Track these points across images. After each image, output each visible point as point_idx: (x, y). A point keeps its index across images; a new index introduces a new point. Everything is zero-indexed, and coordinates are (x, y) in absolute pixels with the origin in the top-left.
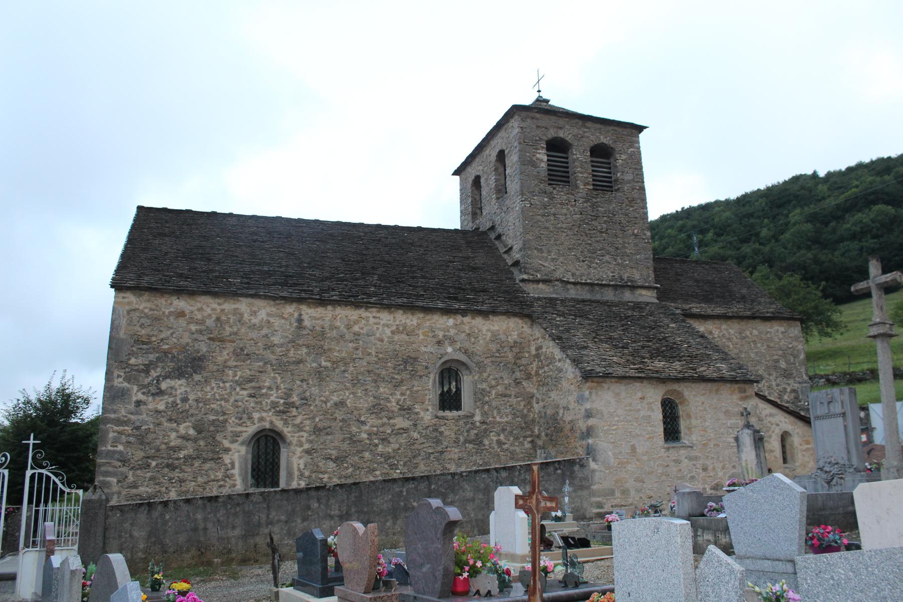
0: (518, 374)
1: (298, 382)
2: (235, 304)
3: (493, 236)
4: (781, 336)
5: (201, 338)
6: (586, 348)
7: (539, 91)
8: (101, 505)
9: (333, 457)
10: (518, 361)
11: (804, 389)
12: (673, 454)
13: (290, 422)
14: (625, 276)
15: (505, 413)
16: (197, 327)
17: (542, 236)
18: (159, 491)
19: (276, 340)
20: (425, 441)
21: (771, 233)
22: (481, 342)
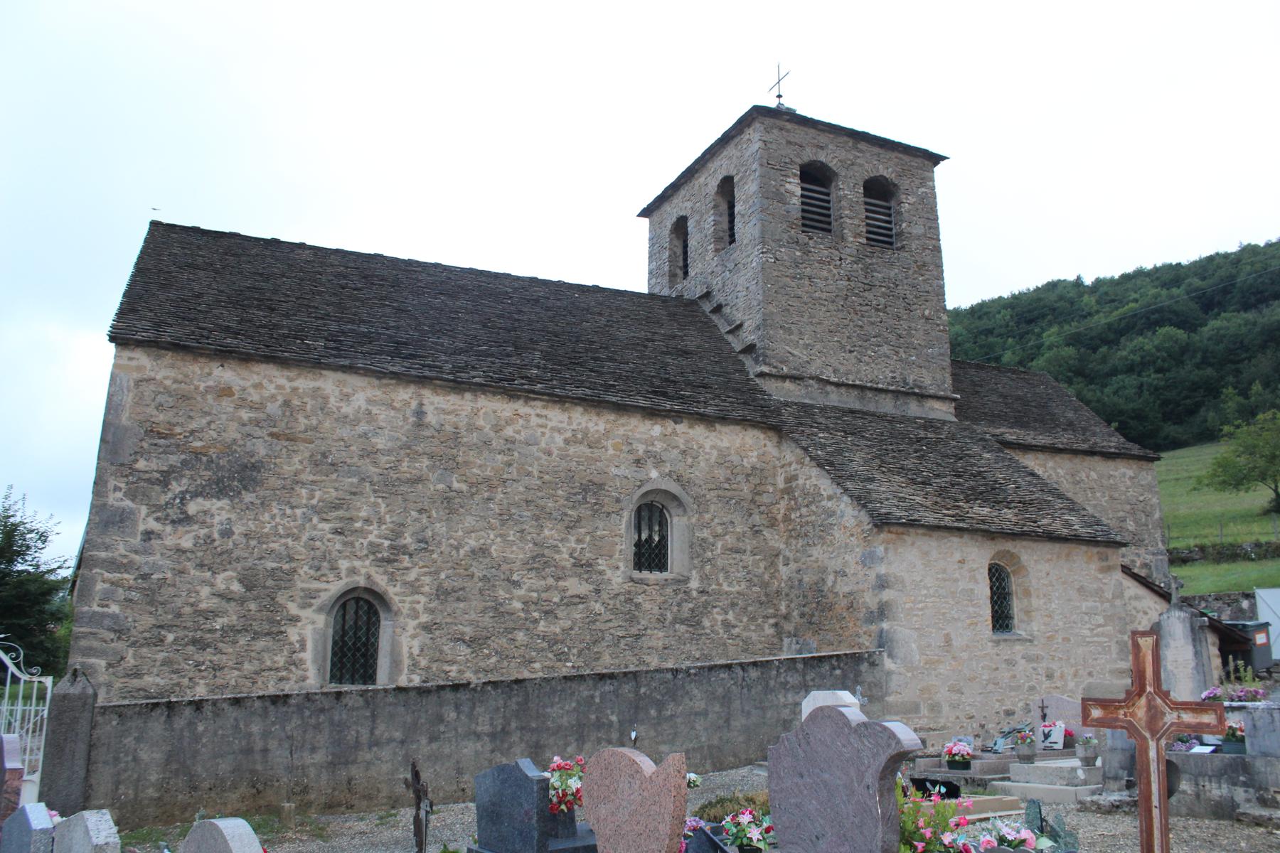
0: (757, 519)
1: (414, 513)
2: (315, 380)
3: (707, 307)
4: (1129, 483)
5: (258, 432)
6: (872, 480)
7: (779, 96)
8: (85, 704)
9: (467, 638)
10: (757, 498)
11: (1159, 563)
12: (1006, 651)
13: (398, 578)
14: (911, 379)
15: (736, 577)
16: (251, 415)
17: (791, 309)
18: (178, 684)
19: (380, 442)
20: (612, 617)
21: (1017, 359)
22: (702, 464)
